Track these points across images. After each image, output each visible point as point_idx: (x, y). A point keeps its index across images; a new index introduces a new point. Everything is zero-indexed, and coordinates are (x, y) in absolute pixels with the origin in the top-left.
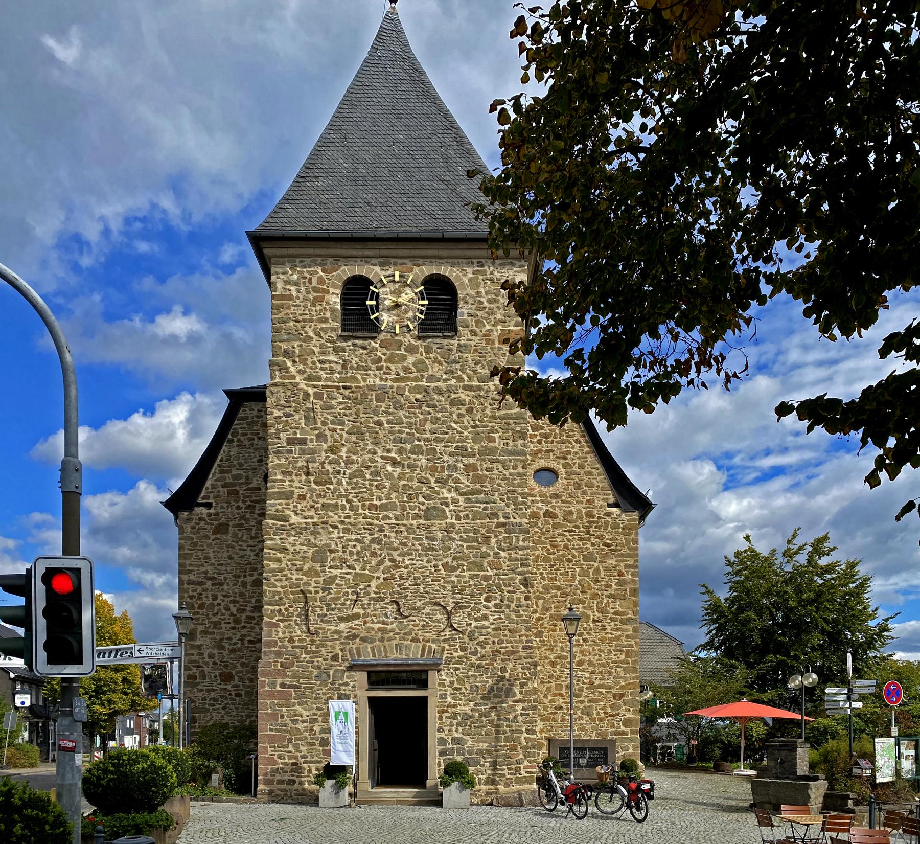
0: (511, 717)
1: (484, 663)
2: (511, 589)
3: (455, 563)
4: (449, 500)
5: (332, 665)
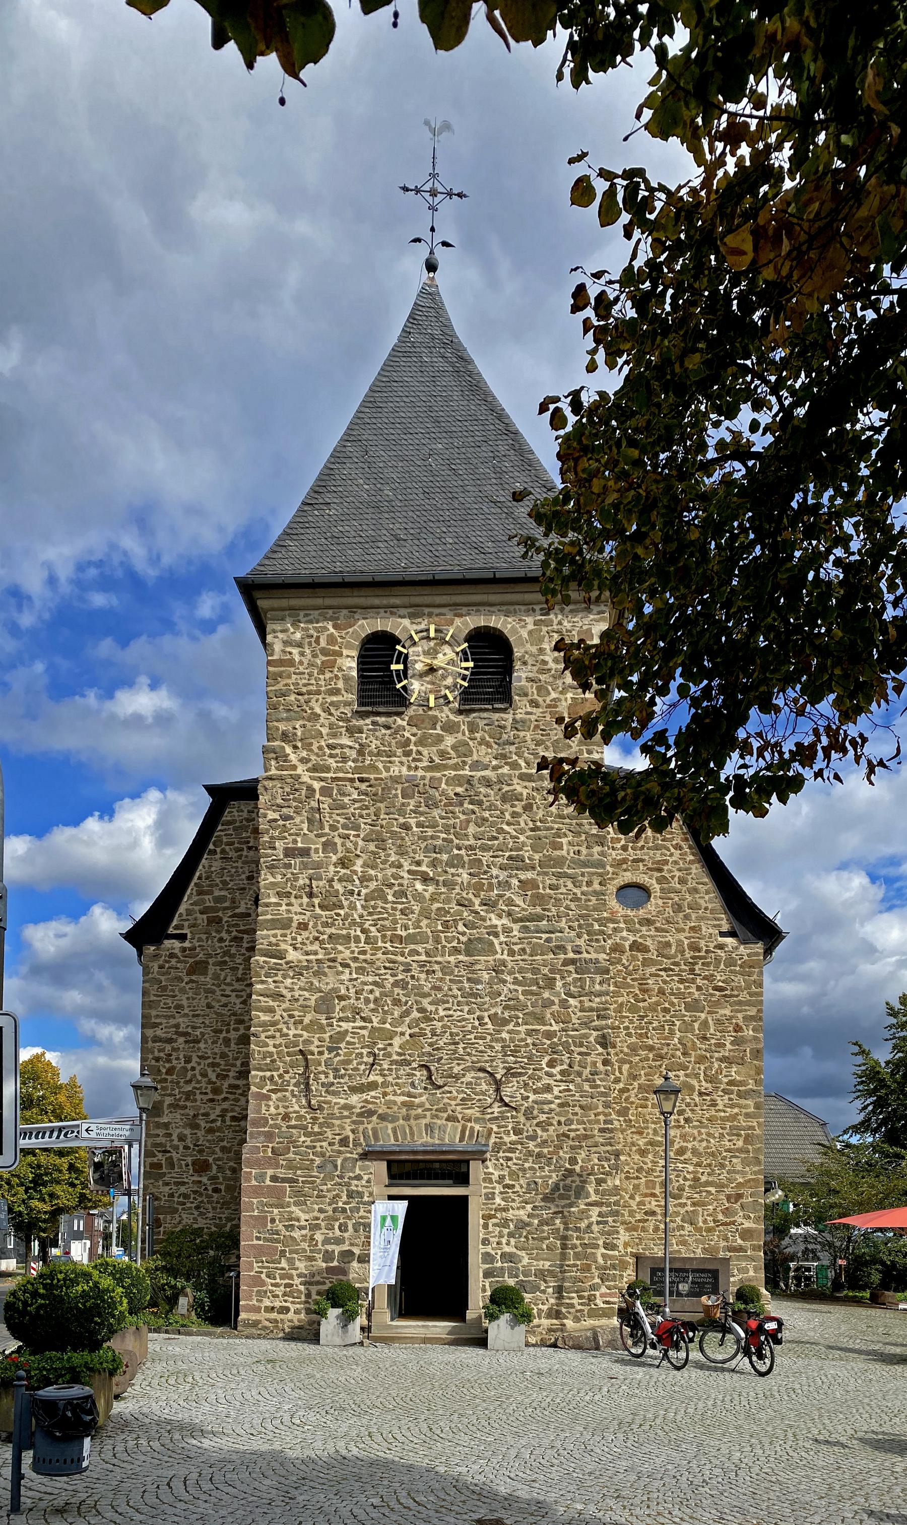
0: (583, 1225)
1: (545, 1151)
2: (583, 1050)
3: (506, 1015)
4: (499, 929)
5: (340, 1152)
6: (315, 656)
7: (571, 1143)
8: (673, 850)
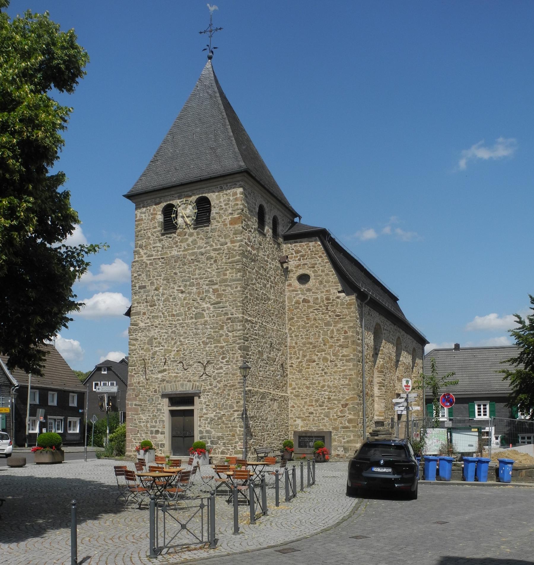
0: (232, 419)
1: (220, 391)
2: (234, 352)
3: (208, 341)
4: (206, 308)
5: (154, 395)
6: (149, 216)
7: (228, 388)
8: (318, 258)
